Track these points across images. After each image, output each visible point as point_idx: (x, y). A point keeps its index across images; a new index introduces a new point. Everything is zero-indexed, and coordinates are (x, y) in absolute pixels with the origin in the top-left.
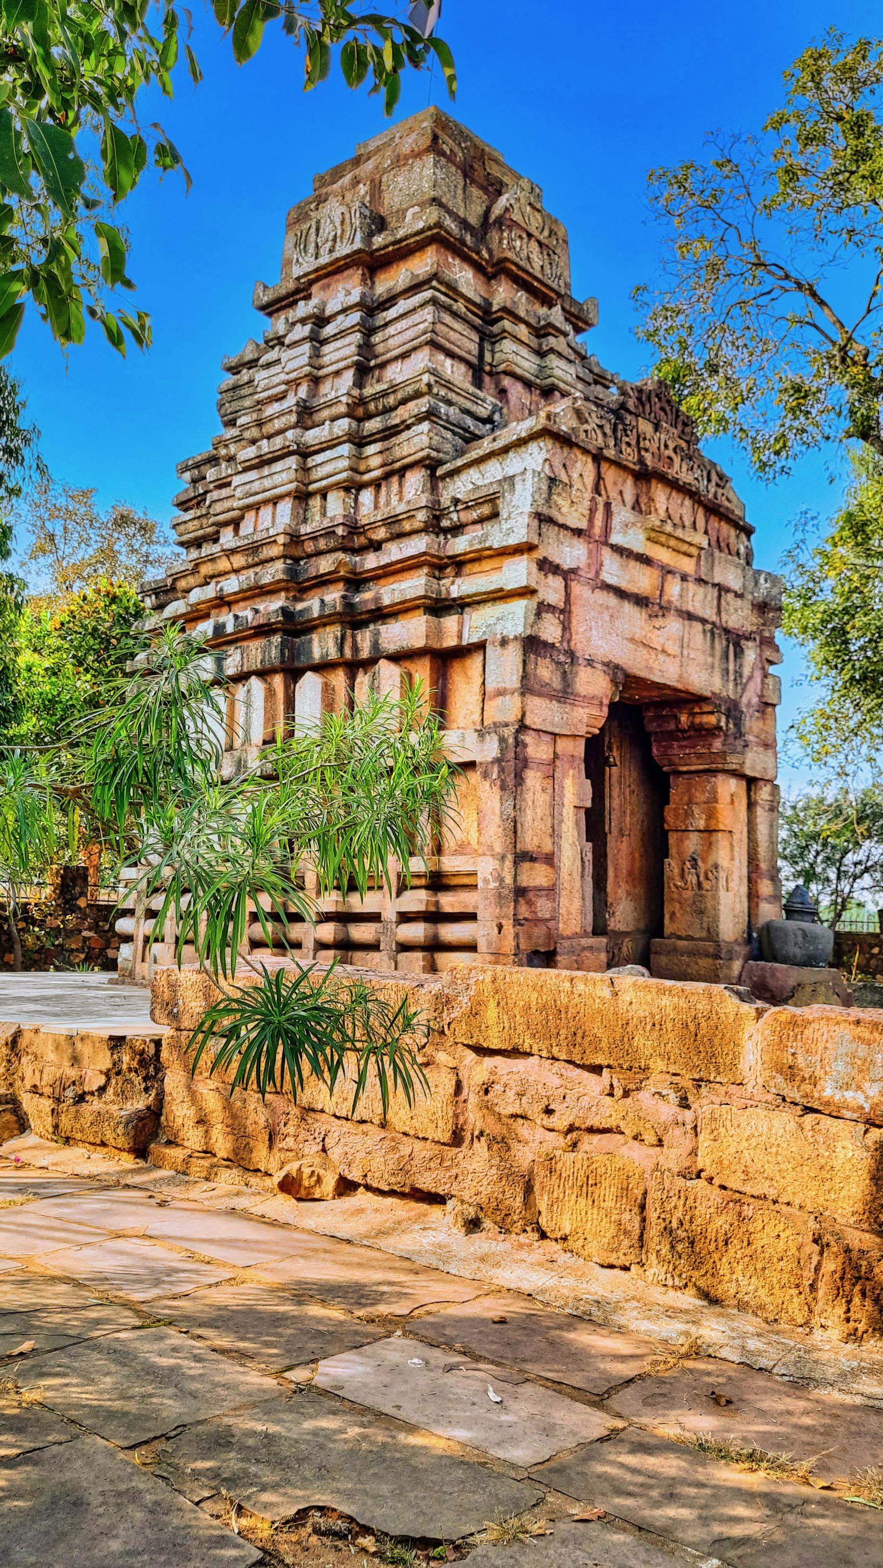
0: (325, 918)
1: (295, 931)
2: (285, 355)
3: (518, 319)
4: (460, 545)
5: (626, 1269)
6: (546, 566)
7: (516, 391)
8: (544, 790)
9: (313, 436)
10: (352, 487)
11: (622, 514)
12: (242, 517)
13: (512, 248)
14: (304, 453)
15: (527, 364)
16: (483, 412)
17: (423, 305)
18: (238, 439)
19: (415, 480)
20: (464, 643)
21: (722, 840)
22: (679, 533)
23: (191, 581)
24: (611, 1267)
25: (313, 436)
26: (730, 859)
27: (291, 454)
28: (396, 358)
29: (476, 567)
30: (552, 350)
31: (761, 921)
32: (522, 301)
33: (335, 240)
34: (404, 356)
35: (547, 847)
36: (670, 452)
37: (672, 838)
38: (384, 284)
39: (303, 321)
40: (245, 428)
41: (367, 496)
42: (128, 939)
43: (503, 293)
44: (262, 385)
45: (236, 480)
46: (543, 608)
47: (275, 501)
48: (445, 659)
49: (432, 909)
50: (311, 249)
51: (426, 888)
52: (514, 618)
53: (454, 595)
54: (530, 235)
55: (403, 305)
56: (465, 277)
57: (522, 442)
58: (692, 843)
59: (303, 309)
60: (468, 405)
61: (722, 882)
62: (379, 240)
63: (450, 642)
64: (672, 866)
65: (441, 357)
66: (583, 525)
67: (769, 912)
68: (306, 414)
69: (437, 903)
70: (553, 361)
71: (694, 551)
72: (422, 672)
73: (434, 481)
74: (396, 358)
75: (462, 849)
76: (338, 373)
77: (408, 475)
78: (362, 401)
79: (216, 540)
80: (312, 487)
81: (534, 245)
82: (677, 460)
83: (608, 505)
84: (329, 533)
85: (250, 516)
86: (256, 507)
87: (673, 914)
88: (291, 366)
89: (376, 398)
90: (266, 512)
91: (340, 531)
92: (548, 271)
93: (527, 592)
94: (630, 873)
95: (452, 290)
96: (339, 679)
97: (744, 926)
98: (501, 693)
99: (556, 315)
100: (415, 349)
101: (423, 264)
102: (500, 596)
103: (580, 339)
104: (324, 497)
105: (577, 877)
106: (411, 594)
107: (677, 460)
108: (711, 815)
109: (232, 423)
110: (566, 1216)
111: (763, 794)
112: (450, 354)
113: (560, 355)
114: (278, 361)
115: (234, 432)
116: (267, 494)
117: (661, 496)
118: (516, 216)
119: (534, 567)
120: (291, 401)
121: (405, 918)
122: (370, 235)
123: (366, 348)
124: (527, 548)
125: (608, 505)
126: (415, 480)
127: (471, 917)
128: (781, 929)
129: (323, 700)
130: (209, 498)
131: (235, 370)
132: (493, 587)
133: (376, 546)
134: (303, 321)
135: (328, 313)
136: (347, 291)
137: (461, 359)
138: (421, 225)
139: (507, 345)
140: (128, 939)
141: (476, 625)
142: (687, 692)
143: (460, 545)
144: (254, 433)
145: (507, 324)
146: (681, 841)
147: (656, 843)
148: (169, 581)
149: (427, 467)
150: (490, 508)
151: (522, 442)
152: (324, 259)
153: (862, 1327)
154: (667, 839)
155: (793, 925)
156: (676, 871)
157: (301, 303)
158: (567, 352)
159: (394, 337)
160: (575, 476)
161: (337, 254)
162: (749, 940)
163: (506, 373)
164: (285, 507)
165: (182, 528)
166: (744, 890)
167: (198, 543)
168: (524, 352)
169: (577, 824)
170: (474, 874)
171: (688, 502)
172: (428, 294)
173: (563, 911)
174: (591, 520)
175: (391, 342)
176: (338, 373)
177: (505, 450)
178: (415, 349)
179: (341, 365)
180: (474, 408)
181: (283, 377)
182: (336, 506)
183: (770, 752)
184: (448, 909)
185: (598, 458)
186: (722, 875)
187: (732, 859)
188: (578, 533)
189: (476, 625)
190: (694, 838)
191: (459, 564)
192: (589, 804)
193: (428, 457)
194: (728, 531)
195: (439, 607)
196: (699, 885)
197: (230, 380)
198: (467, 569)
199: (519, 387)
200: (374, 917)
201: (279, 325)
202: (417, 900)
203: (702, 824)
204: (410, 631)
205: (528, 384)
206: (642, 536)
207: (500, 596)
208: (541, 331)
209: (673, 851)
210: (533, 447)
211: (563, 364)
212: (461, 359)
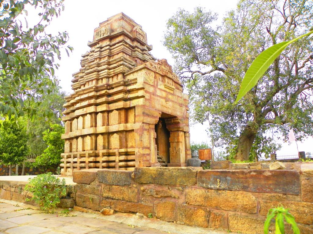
0: (104, 162)
1: (98, 165)
2: (94, 54)
3: (138, 48)
4: (129, 88)
5: (173, 222)
6: (146, 92)
7: (138, 61)
8: (147, 135)
9: (100, 68)
10: (108, 78)
11: (160, 83)
12: (85, 84)
13: (137, 36)
14: (99, 71)
15: (140, 56)
16: (133, 64)
17: (121, 45)
18: (85, 69)
19: (120, 76)
20: (131, 106)
21: (180, 144)
22: (170, 86)
23: (76, 95)
24: (170, 222)
25: (100, 68)
26: (182, 147)
27: (95, 72)
28: (116, 54)
29: (133, 92)
30: (145, 54)
31: (188, 159)
32: (138, 45)
33: (104, 34)
34: (118, 54)
35: (149, 146)
36: (167, 72)
37: (171, 144)
38: (113, 42)
39: (98, 48)
40: (87, 67)
41: (111, 79)
42: (63, 168)
43: (136, 44)
44: (89, 59)
45: (84, 77)
46: (146, 99)
47: (92, 80)
48: (127, 110)
49: (126, 159)
50: (99, 35)
51: (125, 155)
52: (140, 101)
53: (129, 97)
54: (140, 34)
55: (117, 45)
56: (128, 41)
57: (140, 70)
58: (175, 144)
59: (98, 46)
60: (130, 63)
61: (181, 152)
62: (112, 34)
63: (128, 106)
64: (171, 149)
65: (125, 54)
66: (153, 84)
67: (189, 157)
68: (99, 65)
69: (127, 158)
70: (145, 55)
71: (173, 89)
72: (123, 113)
73: (124, 77)
74: (116, 54)
75: (132, 147)
76: (105, 57)
77: (119, 75)
78: (109, 62)
79: (80, 88)
80: (100, 78)
81: (141, 35)
82: (169, 73)
83: (157, 81)
84: (104, 86)
85: (87, 83)
86: (89, 82)
87: (172, 158)
88: (95, 56)
89: (112, 61)
90: (90, 83)
91: (106, 86)
92: (143, 40)
93: (143, 97)
94: (163, 151)
95: (126, 43)
96: (106, 114)
97: (184, 160)
98: (138, 115)
99: (145, 48)
100: (119, 53)
101: (121, 38)
102: (138, 97)
103: (150, 52)
104: (102, 79)
105: (154, 152)
106: (120, 97)
107: (169, 73)
108: (178, 139)
109: (84, 66)
110: (161, 213)
111: (187, 135)
112: (126, 54)
113: (146, 54)
114: (93, 55)
115: (84, 68)
116: (91, 79)
117: (167, 80)
118: (138, 31)
119: (144, 92)
120: (95, 62)
121: (121, 161)
122: (111, 33)
123: (110, 52)
124: (143, 88)
125: (157, 81)
126: (120, 76)
127: (134, 160)
128: (192, 160)
129: (102, 118)
130: (79, 80)
131: (84, 57)
132: (136, 96)
133: (113, 88)
134: (98, 48)
135: (103, 46)
136: (107, 42)
137: (128, 55)
138: (120, 31)
139: (137, 52)
140: (63, 168)
141: (134, 103)
142: (173, 116)
143: (129, 88)
144: (88, 68)
145: (136, 49)
146: (173, 144)
147: (168, 145)
148: (71, 96)
149: (122, 74)
150: (135, 81)
151: (140, 70)
152: (102, 37)
153: (217, 227)
154: (170, 144)
155: (193, 159)
156: (172, 150)
157: (97, 45)
158: (148, 54)
159: (115, 50)
160: (151, 75)
161: (104, 36)
162: (186, 163)
163: (136, 57)
164: (94, 82)
165: (73, 86)
166: (184, 153)
167: (76, 89)
168: (140, 54)
169: (154, 141)
170: (134, 152)
171: (171, 81)
172: (122, 43)
173: (152, 158)
174: (154, 83)
175: (114, 52)
176: (105, 57)
177: (137, 71)
178: (119, 53)
179: (105, 55)
180: (131, 63)
181: (94, 58)
182: (105, 81)
183: (188, 127)
184: (129, 159)
185: (155, 72)
186: (181, 150)
187: (182, 147)
188: (152, 86)
189: (134, 103)
190: (175, 143)
191: (129, 92)
192: (156, 137)
193: (123, 72)
194: (179, 86)
195: (109, 103)
196: (176, 152)
197: (83, 58)
198: (131, 92)
199: (139, 60)
200: (114, 161)
201: (93, 49)
202: (123, 158)
203: (176, 141)
204: (120, 104)
205: (140, 59)
206: (164, 87)
207: (138, 97)
208: (143, 50)
209: (171, 146)
210: (143, 70)
211: (147, 56)
212: (128, 55)
